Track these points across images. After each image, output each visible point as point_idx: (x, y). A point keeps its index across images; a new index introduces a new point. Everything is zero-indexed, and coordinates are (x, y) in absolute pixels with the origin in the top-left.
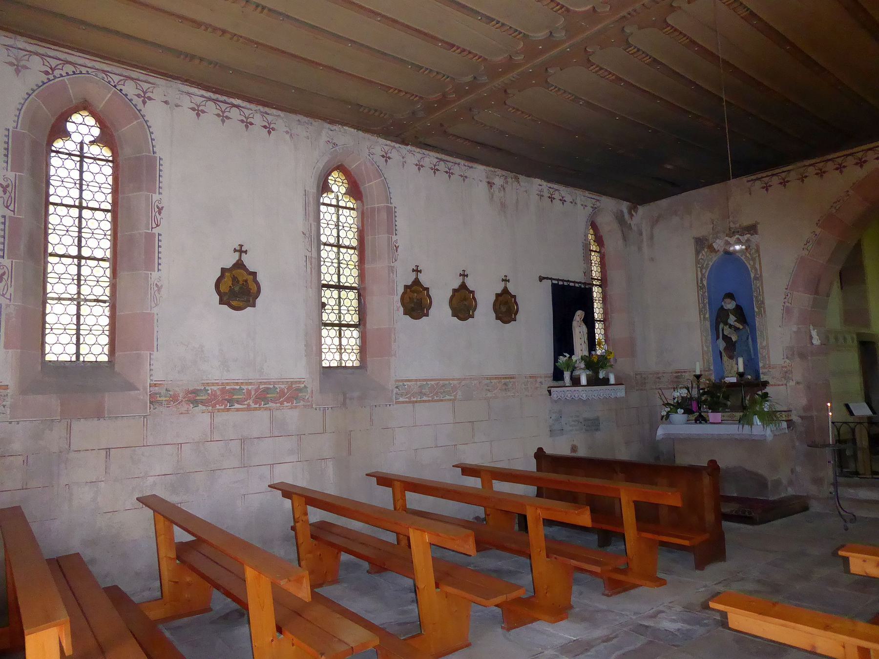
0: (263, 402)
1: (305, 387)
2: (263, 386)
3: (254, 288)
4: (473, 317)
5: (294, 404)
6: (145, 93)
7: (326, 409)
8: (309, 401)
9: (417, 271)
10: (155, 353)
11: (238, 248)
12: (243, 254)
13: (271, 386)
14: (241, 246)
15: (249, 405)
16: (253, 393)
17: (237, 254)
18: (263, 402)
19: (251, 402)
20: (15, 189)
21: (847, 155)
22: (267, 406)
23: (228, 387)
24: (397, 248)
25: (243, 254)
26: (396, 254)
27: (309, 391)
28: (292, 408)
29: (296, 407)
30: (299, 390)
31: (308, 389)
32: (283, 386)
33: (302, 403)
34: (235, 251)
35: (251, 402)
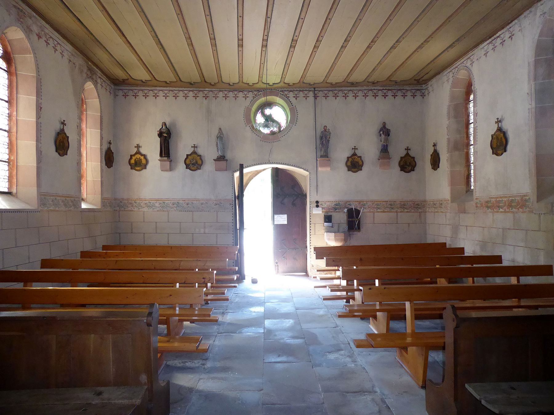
0: (510, 208)
1: (529, 199)
2: (511, 198)
3: (361, 163)
4: (186, 169)
5: (524, 210)
6: (125, 94)
7: (541, 214)
8: (531, 209)
9: (63, 123)
10: (477, 184)
11: (354, 148)
12: (195, 148)
13: (514, 198)
14: (408, 147)
15: (505, 209)
16: (507, 202)
17: (407, 150)
18: (510, 208)
19: (505, 208)
20: (165, 144)
21: (389, 90)
22: (512, 210)
23: (498, 199)
24: (41, 108)
25: (409, 150)
26: (40, 113)
27: (531, 200)
28: (523, 213)
29: (525, 212)
30: (526, 201)
31: (531, 200)
32: (518, 198)
33: (528, 209)
34: (192, 147)
35: (505, 208)
